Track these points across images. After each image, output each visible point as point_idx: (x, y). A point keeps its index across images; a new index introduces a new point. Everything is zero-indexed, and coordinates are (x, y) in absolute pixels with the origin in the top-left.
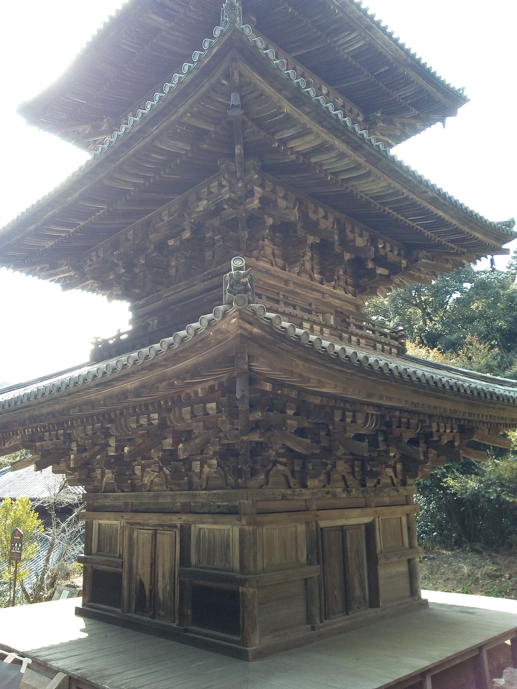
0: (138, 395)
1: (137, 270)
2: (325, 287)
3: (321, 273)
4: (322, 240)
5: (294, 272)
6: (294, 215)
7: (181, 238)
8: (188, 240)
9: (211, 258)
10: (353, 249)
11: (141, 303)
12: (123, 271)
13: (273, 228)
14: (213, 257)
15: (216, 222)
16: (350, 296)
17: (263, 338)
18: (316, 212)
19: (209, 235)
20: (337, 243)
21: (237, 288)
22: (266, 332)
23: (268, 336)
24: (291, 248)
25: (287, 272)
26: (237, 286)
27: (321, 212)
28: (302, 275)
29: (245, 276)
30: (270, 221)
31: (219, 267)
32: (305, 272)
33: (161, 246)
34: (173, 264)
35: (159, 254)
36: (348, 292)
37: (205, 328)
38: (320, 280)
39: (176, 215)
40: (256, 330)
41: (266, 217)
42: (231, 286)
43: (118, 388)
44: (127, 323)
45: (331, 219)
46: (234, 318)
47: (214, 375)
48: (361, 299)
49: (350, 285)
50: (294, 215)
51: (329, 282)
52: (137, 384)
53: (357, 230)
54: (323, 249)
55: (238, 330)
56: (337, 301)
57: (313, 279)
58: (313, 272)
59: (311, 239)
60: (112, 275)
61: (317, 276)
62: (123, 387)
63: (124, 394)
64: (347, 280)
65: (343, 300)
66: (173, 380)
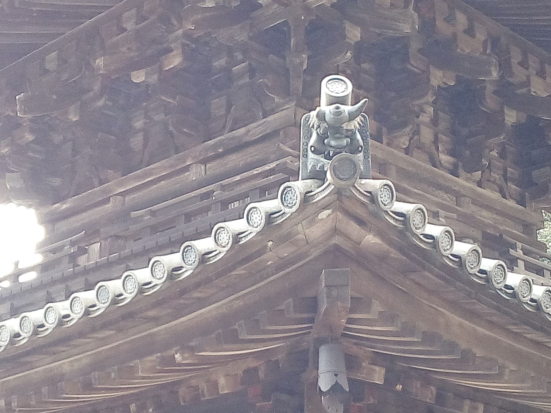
0: (88, 387)
1: (57, 138)
2: (463, 182)
3: (452, 153)
4: (459, 80)
5: (397, 147)
6: (408, 25)
7: (161, 68)
8: (175, 72)
9: (223, 112)
10: (526, 103)
11: (64, 206)
12: (30, 137)
13: (359, 49)
14: (228, 110)
15: (240, 34)
16: (511, 203)
17: (383, 258)
18: (450, 19)
19: (220, 63)
20: (490, 88)
21: (333, 143)
22: (390, 243)
23: (394, 254)
24: (393, 94)
25: (384, 146)
26: (336, 139)
27: (461, 19)
28: (414, 154)
29: (352, 117)
30: (354, 34)
31: (242, 131)
32: (420, 147)
33: (116, 84)
34: (139, 124)
35: (110, 104)
36: (508, 197)
37: (259, 229)
38: (451, 167)
39: (153, 17)
40: (371, 239)
41: (348, 25)
42: (321, 138)
43: (43, 367)
44: (34, 247)
45: (481, 36)
46: (324, 209)
47: (263, 340)
48: (535, 211)
49: (513, 181)
50: (408, 25)
51: (470, 170)
52: (85, 361)
53: (533, 62)
54: (461, 102)
55: (331, 237)
56: (485, 213)
57: (438, 164)
58: (437, 149)
59: (438, 78)
60: (7, 146)
61: (445, 158)
62: (51, 369)
63: (54, 381)
64: (505, 171)
65: (498, 212)
66: (172, 352)
